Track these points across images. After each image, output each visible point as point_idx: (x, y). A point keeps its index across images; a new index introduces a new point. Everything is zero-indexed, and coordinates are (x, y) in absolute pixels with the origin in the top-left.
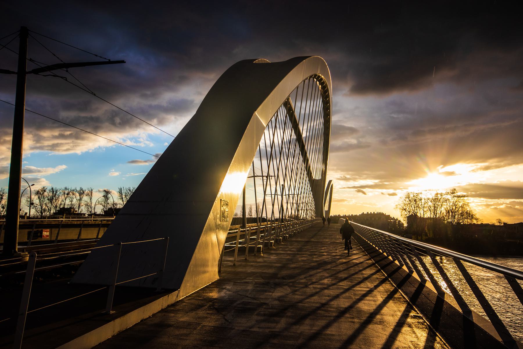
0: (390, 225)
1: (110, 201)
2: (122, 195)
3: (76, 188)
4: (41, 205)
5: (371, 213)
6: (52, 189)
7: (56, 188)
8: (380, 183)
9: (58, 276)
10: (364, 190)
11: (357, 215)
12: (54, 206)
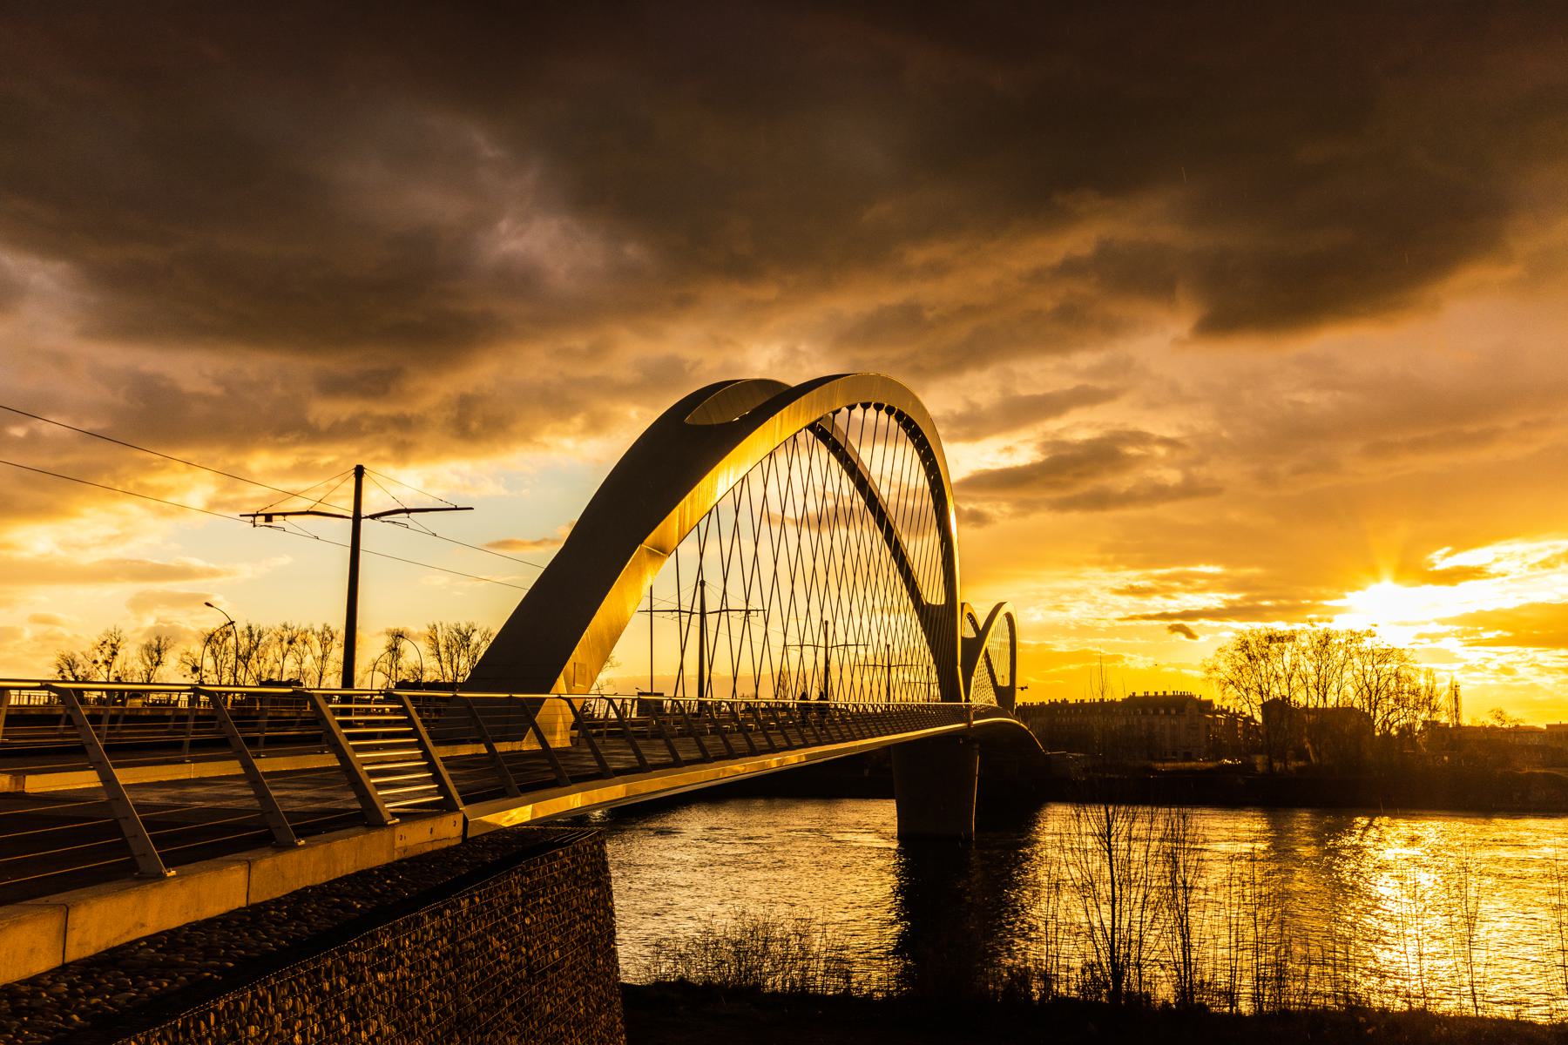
0: (1213, 728)
1: (406, 661)
2: (438, 644)
3: (312, 625)
4: (219, 673)
5: (1156, 693)
6: (250, 628)
7: (259, 626)
8: (1248, 604)
9: (231, 965)
10: (1187, 623)
11: (1117, 700)
12: (254, 674)
